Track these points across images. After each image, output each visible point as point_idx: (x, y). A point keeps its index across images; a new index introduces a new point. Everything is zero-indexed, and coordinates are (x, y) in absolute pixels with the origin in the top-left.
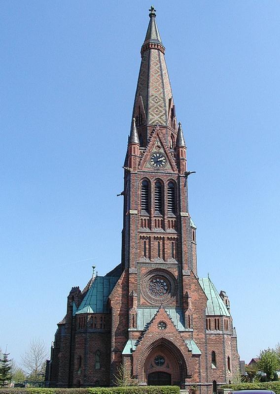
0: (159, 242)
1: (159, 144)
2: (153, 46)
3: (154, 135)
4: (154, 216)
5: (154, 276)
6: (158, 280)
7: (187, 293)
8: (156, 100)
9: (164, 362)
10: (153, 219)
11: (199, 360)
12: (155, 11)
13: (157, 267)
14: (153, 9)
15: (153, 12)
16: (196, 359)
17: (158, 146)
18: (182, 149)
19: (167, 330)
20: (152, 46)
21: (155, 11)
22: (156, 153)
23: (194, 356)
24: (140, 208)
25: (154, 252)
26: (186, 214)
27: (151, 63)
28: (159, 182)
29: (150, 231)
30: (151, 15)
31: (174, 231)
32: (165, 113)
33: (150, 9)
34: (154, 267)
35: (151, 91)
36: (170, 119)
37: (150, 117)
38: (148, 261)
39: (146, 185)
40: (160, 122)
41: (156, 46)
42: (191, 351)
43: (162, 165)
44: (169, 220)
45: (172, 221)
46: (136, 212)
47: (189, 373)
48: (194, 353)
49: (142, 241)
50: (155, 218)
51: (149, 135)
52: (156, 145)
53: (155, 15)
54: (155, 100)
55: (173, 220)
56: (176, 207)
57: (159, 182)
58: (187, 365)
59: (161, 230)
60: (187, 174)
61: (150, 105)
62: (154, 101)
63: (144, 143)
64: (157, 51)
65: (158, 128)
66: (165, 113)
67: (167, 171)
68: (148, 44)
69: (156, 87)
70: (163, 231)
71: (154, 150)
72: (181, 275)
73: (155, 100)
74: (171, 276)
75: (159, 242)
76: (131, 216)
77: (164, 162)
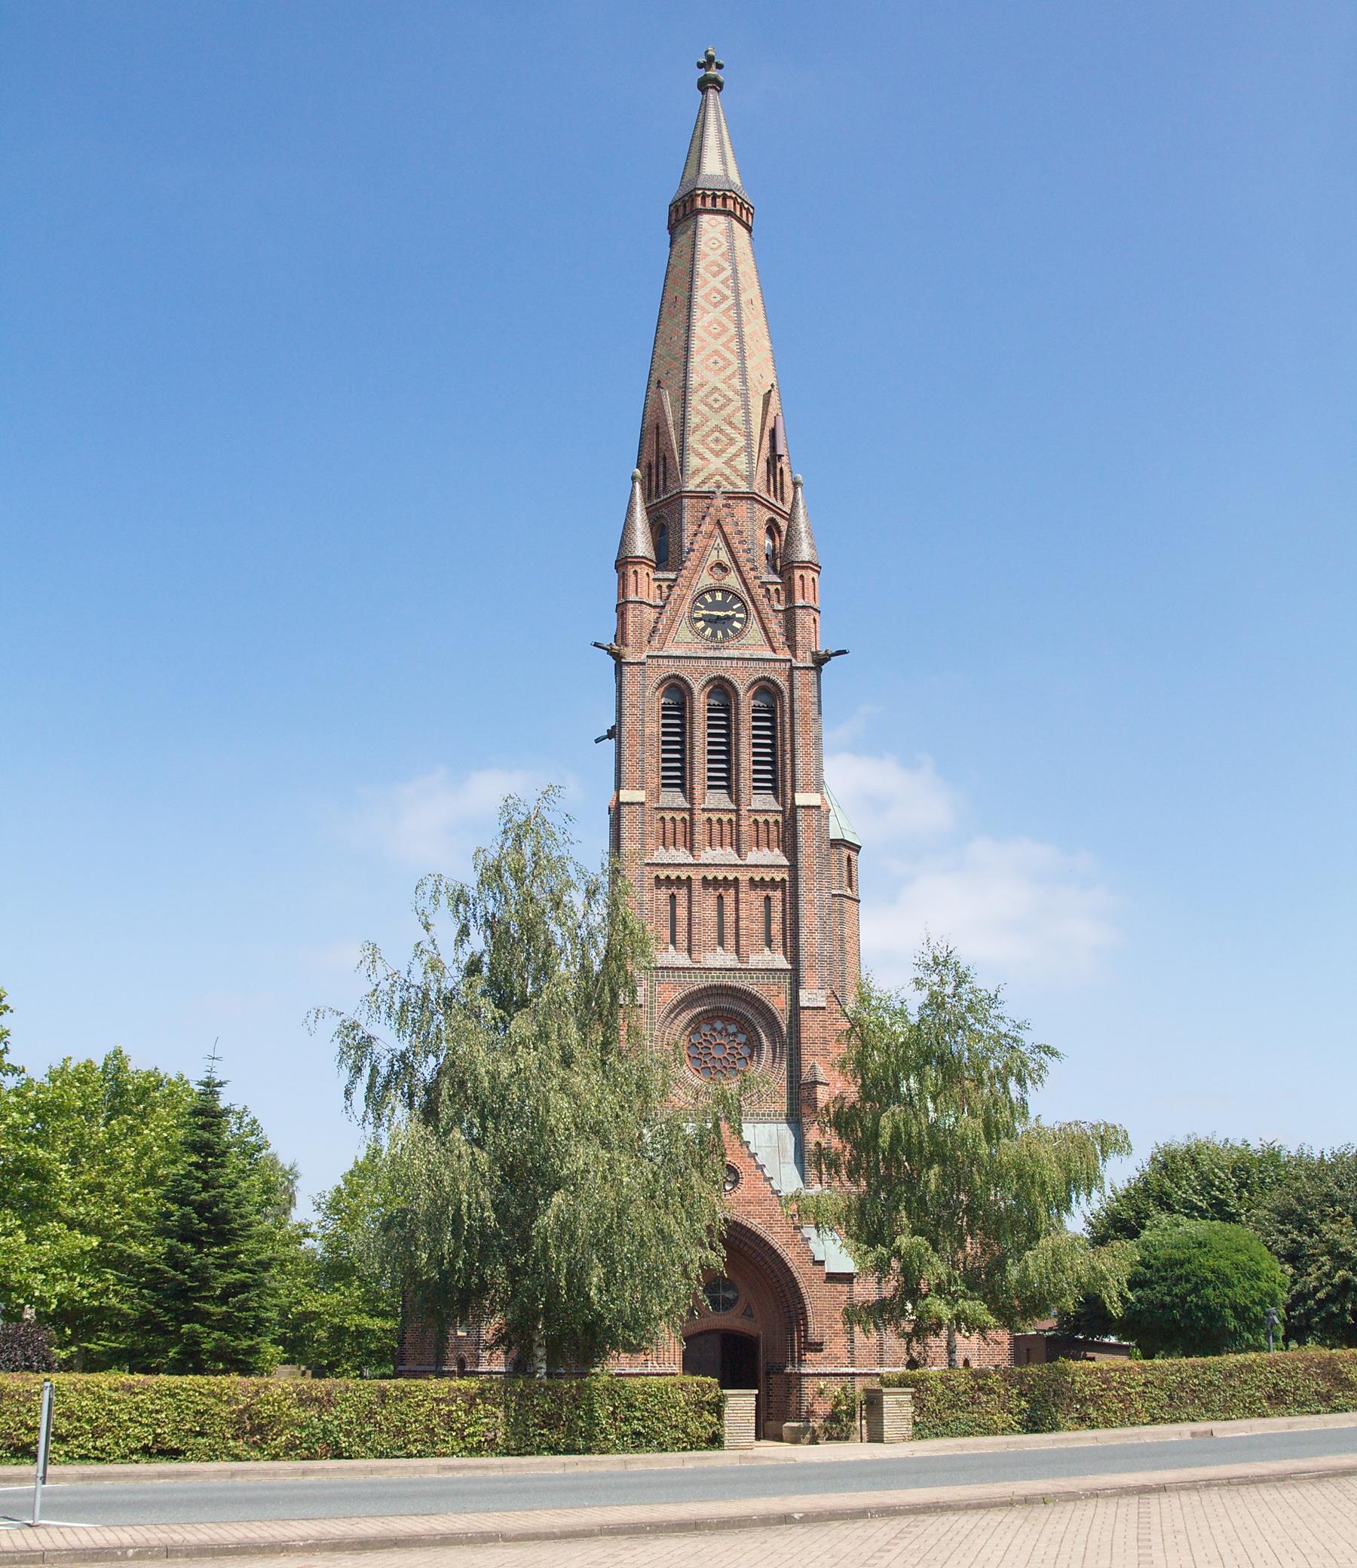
0: (720, 897)
1: (724, 557)
2: (709, 201)
3: (707, 526)
4: (704, 810)
5: (706, 1011)
6: (719, 1025)
7: (813, 1066)
8: (716, 400)
9: (736, 1299)
10: (701, 817)
11: (851, 1291)
12: (719, 67)
13: (716, 982)
14: (710, 59)
15: (713, 72)
16: (839, 1287)
17: (719, 565)
18: (803, 572)
19: (742, 1191)
20: (704, 203)
21: (719, 67)
22: (711, 591)
23: (832, 1278)
24: (654, 781)
25: (706, 932)
26: (813, 799)
27: (701, 267)
28: (722, 689)
29: (691, 860)
30: (704, 85)
31: (777, 857)
32: (748, 447)
33: (703, 60)
34: (701, 982)
35: (701, 371)
36: (763, 466)
37: (693, 462)
38: (682, 960)
39: (677, 692)
40: (727, 479)
41: (719, 201)
42: (821, 1263)
43: (734, 630)
44: (756, 822)
45: (766, 822)
46: (639, 796)
47: (814, 1335)
48: (831, 1267)
49: (663, 894)
50: (706, 815)
51: (689, 529)
52: (713, 559)
53: (718, 85)
54: (710, 400)
55: (714, 819)
56: (776, 776)
57: (722, 689)
58: (809, 1307)
59: (728, 855)
60: (820, 661)
61: (694, 420)
62: (725, 359)
63: (667, 553)
64: (721, 218)
65: (719, 501)
66: (748, 447)
67: (750, 652)
68: (691, 196)
69: (716, 352)
70: (734, 859)
71: (706, 580)
72: (796, 1009)
73: (710, 400)
74: (749, 1003)
75: (720, 897)
76: (800, 814)
77: (739, 620)
